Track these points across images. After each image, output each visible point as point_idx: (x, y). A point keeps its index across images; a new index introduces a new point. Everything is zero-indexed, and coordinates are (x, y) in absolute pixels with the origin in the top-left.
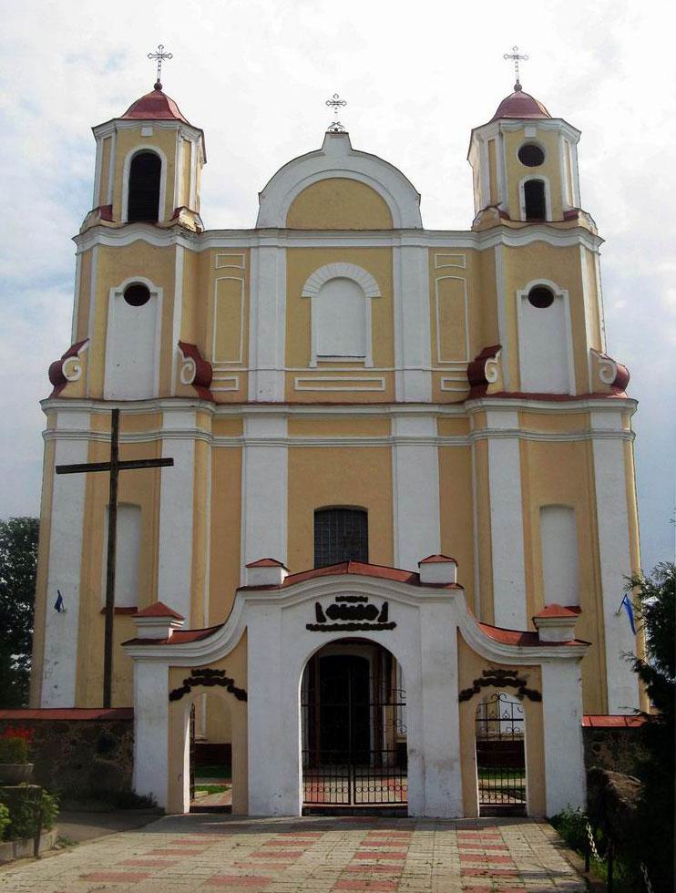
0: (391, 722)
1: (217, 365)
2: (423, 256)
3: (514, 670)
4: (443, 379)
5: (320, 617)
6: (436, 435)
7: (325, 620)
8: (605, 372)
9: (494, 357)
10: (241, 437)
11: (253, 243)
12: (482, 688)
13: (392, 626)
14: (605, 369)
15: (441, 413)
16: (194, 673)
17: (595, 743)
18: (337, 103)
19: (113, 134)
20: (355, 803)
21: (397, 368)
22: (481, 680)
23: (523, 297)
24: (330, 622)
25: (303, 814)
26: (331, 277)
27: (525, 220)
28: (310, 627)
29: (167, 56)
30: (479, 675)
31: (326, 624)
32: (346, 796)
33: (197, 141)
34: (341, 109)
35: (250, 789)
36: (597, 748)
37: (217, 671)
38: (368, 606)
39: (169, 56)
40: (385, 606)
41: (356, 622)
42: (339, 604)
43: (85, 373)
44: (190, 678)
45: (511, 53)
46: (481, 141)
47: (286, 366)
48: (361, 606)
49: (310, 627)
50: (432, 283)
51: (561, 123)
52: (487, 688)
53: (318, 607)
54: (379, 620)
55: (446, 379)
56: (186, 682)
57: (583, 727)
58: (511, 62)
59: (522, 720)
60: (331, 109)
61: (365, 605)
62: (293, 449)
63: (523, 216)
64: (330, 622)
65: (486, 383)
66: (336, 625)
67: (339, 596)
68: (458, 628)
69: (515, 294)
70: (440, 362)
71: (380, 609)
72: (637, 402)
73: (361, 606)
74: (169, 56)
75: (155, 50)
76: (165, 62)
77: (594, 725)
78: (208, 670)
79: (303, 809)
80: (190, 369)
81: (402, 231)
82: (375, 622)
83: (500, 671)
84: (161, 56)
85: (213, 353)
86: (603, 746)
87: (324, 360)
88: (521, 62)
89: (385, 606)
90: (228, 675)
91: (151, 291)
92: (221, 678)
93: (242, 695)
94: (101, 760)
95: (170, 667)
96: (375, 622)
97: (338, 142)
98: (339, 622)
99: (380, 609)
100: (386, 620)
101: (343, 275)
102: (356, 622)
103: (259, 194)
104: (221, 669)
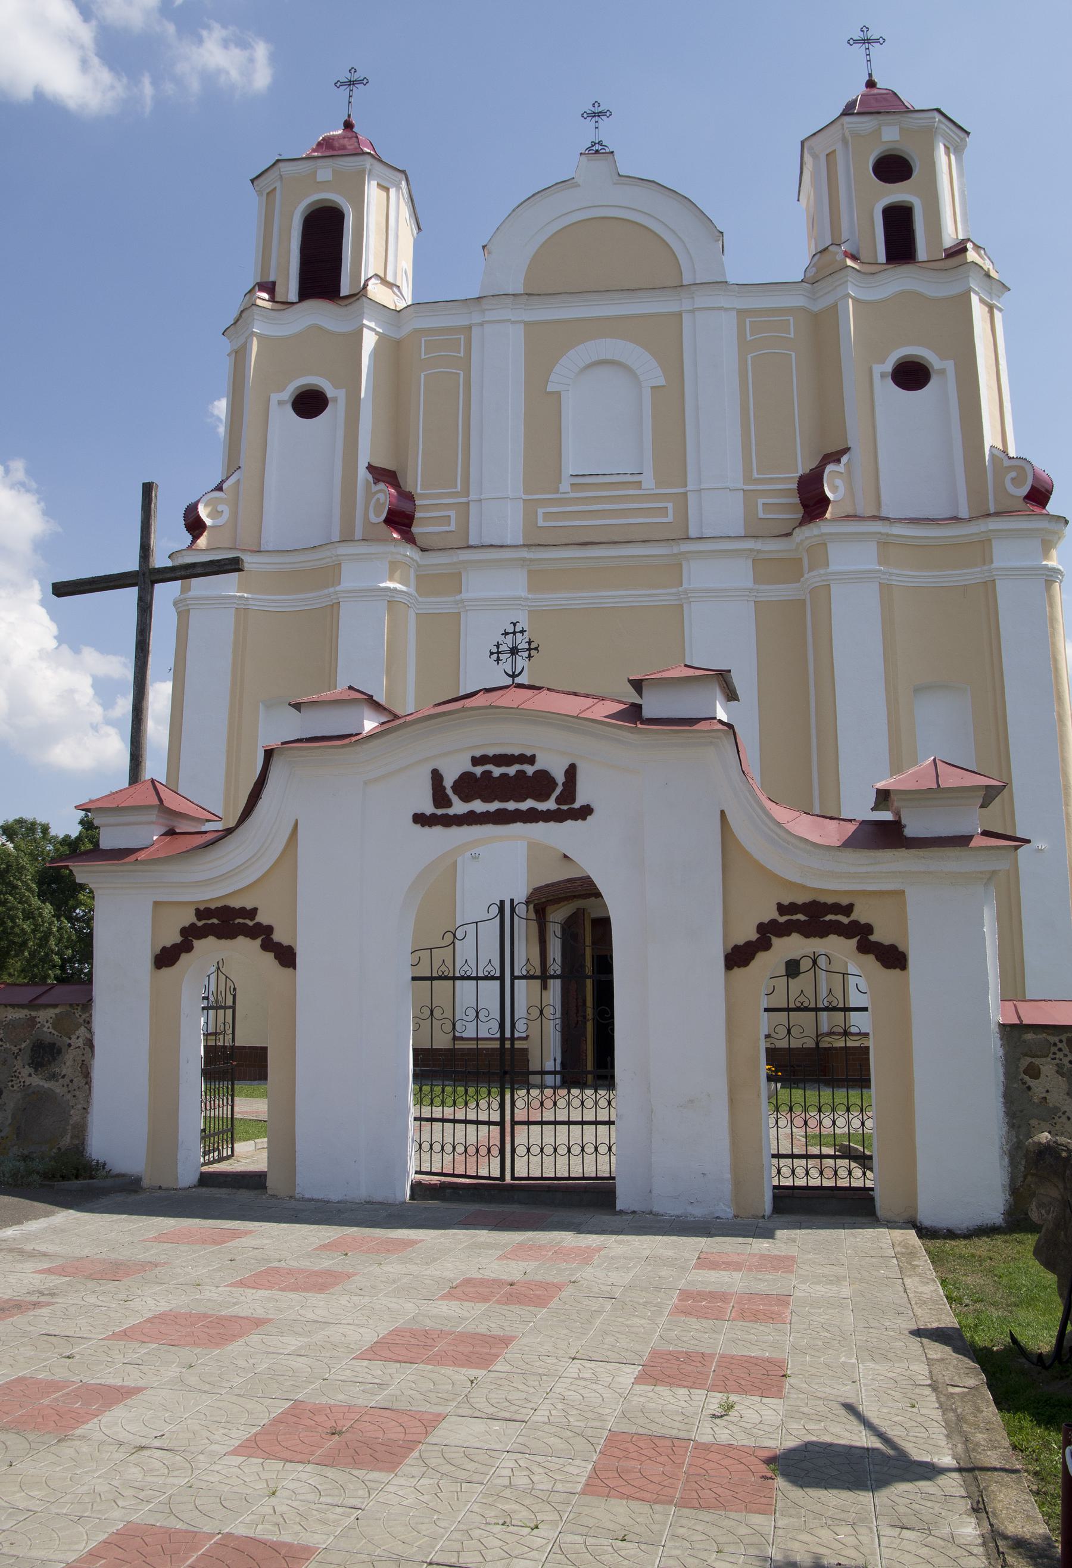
0: (536, 1013)
1: (424, 496)
2: (728, 324)
3: (845, 902)
4: (760, 502)
5: (440, 798)
6: (750, 584)
7: (449, 804)
8: (1013, 479)
9: (838, 461)
10: (458, 597)
11: (476, 318)
12: (775, 941)
13: (586, 812)
14: (1013, 474)
15: (759, 551)
16: (201, 914)
17: (1029, 1060)
18: (599, 114)
19: (278, 184)
20: (513, 1178)
21: (688, 488)
22: (773, 922)
23: (883, 375)
24: (459, 807)
25: (412, 1198)
26: (595, 358)
27: (885, 261)
28: (420, 819)
29: (360, 82)
30: (769, 913)
31: (451, 811)
32: (496, 1162)
33: (398, 188)
34: (604, 122)
35: (298, 1147)
36: (1034, 1072)
37: (243, 909)
38: (536, 773)
39: (363, 82)
40: (571, 772)
41: (511, 806)
42: (478, 770)
43: (234, 515)
44: (193, 925)
45: (858, 35)
46: (815, 157)
47: (525, 493)
48: (521, 773)
49: (420, 819)
50: (743, 362)
51: (938, 117)
52: (785, 939)
53: (437, 777)
54: (558, 801)
55: (755, 471)
56: (184, 931)
57: (1000, 1024)
58: (859, 50)
59: (865, 1009)
60: (590, 123)
61: (530, 770)
62: (529, 611)
63: (882, 257)
64: (459, 807)
65: (826, 501)
66: (472, 813)
67: (478, 754)
68: (722, 812)
69: (870, 370)
70: (755, 475)
71: (560, 778)
72: (1067, 522)
73: (521, 773)
74: (363, 82)
75: (344, 76)
76: (359, 90)
77: (1025, 1022)
78: (226, 908)
79: (413, 1187)
80: (382, 501)
81: (694, 288)
82: (550, 805)
83: (814, 904)
84: (351, 83)
85: (416, 482)
86: (1047, 1068)
87: (580, 481)
88: (875, 48)
89: (571, 772)
90: (262, 918)
91: (329, 396)
92: (251, 923)
93: (286, 957)
94: (36, 1081)
95: (156, 904)
96: (550, 805)
97: (599, 165)
98: (478, 806)
99: (560, 778)
100: (573, 801)
101: (609, 357)
102: (511, 806)
103: (484, 247)
104: (249, 906)
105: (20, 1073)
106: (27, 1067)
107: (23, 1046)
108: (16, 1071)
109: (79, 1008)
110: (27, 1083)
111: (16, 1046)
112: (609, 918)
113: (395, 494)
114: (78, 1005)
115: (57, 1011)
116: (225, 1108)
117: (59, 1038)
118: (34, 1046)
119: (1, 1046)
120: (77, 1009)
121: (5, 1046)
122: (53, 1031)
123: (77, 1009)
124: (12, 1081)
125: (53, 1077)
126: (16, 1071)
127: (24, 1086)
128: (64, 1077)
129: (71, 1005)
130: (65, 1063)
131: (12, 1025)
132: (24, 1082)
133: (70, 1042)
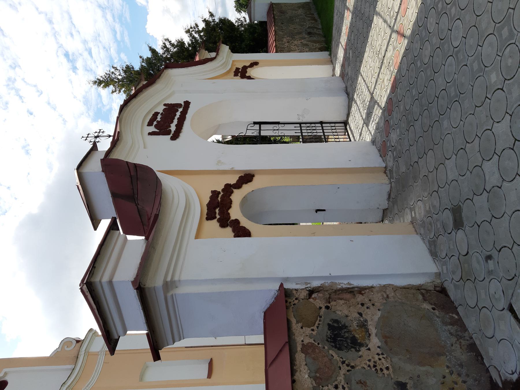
44: (219, 221)
61: (159, 118)
94: (375, 342)
105: (370, 361)
106: (360, 353)
107: (338, 359)
108: (369, 366)
109: (289, 300)
110: (379, 351)
111: (340, 368)
112: (267, 53)
113: (132, 94)
114: (286, 301)
115: (294, 321)
116: (337, 128)
117: (322, 319)
118: (336, 347)
119: (344, 388)
120: (290, 303)
121: (343, 383)
122: (316, 325)
123: (290, 303)
124: (381, 370)
125: (363, 325)
126: (369, 366)
127: (382, 354)
128: (360, 314)
129: (287, 308)
130: (347, 316)
131: (316, 372)
132: (378, 354)
133: (324, 307)
